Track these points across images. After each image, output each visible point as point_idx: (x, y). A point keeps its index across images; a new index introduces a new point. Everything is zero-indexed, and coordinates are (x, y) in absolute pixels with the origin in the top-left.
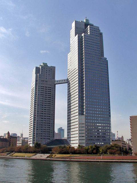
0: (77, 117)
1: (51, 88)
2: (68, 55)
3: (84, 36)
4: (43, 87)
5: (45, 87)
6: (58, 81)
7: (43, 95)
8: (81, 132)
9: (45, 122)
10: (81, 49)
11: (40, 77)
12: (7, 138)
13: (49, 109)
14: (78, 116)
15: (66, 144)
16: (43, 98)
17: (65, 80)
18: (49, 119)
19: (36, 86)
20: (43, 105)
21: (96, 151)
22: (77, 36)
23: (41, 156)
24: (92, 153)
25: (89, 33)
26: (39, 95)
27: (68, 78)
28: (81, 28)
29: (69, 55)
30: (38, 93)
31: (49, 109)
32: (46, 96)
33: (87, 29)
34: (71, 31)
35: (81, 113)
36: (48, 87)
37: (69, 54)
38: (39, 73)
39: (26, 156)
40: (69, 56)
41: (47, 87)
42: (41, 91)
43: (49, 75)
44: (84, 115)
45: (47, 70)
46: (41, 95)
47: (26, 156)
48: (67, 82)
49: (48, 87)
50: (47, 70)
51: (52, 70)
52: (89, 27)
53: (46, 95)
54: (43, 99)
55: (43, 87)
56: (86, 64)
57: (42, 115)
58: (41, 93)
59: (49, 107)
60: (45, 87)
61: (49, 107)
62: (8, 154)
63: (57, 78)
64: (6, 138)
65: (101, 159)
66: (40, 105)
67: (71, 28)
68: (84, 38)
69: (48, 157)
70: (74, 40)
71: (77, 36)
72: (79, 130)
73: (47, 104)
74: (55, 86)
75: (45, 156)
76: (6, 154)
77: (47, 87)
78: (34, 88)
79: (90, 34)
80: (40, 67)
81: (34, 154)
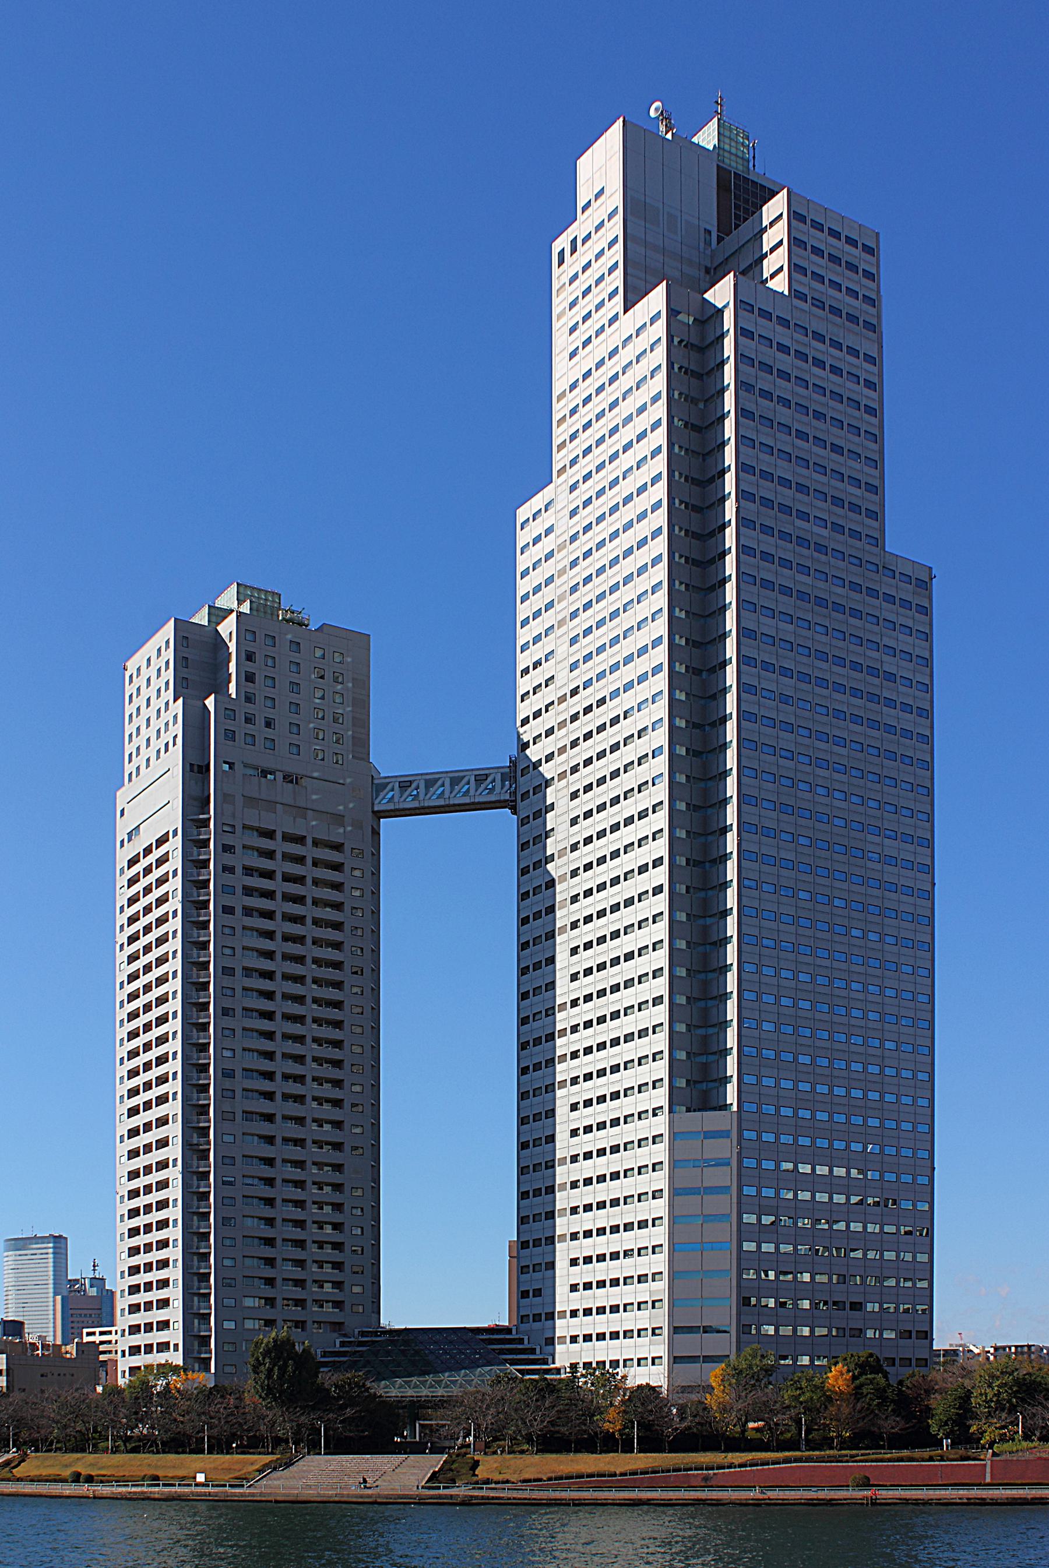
0: (660, 1124)
1: (338, 847)
2: (523, 513)
3: (740, 304)
4: (270, 834)
5: (288, 838)
6: (405, 784)
7: (269, 915)
8: (691, 1344)
9: (293, 1130)
10: (702, 350)
11: (227, 735)
13: (327, 894)
14: (663, 1119)
15: (513, 1362)
16: (267, 945)
17: (481, 778)
18: (329, 1061)
19: (194, 802)
20: (269, 1016)
22: (657, 299)
25: (780, 284)
26: (228, 910)
27: (534, 753)
28: (688, 232)
30: (223, 889)
31: (327, 894)
32: (296, 1029)
33: (746, 230)
34: (562, 243)
35: (695, 1083)
36: (316, 843)
37: (537, 502)
38: (219, 687)
39: (201, 1478)
40: (537, 528)
41: (300, 840)
44: (725, 1107)
46: (248, 911)
47: (201, 1478)
48: (518, 789)
49: (316, 843)
51: (343, 660)
52: (776, 206)
53: (299, 920)
54: (269, 955)
55: (270, 834)
56: (751, 482)
57: (266, 1106)
58: (248, 891)
59: (332, 994)
60: (288, 838)
61: (332, 994)
63: (389, 758)
65: (988, 1480)
68: (741, 332)
70: (607, 355)
71: (657, 299)
72: (675, 1330)
73: (311, 1010)
74: (376, 833)
77: (300, 840)
78: (175, 845)
79: (795, 293)
80: (228, 628)
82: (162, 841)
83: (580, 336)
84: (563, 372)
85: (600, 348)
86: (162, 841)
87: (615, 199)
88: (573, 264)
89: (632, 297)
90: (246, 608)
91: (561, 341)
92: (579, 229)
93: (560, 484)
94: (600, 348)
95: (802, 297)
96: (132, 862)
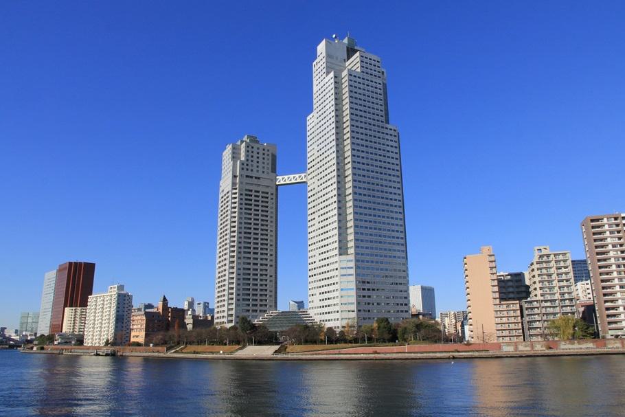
2: (308, 118)
5: (256, 191)
12: (161, 311)
21: (392, 335)
23: (199, 304)
24: (383, 341)
29: (312, 120)
34: (315, 63)
37: (311, 116)
42: (245, 233)
43: (264, 159)
45: (258, 167)
47: (221, 352)
50: (258, 158)
55: (251, 191)
60: (256, 191)
62: (168, 349)
64: (159, 313)
66: (244, 257)
67: (306, 104)
69: (276, 352)
71: (332, 74)
75: (267, 351)
76: (165, 349)
81: (238, 347)
82: (228, 193)
83: (318, 82)
84: (315, 89)
85: (322, 84)
86: (228, 193)
87: (324, 54)
88: (317, 67)
89: (327, 75)
90: (248, 141)
91: (315, 83)
92: (317, 60)
93: (315, 112)
94: (322, 84)
95: (363, 72)
96: (222, 197)
